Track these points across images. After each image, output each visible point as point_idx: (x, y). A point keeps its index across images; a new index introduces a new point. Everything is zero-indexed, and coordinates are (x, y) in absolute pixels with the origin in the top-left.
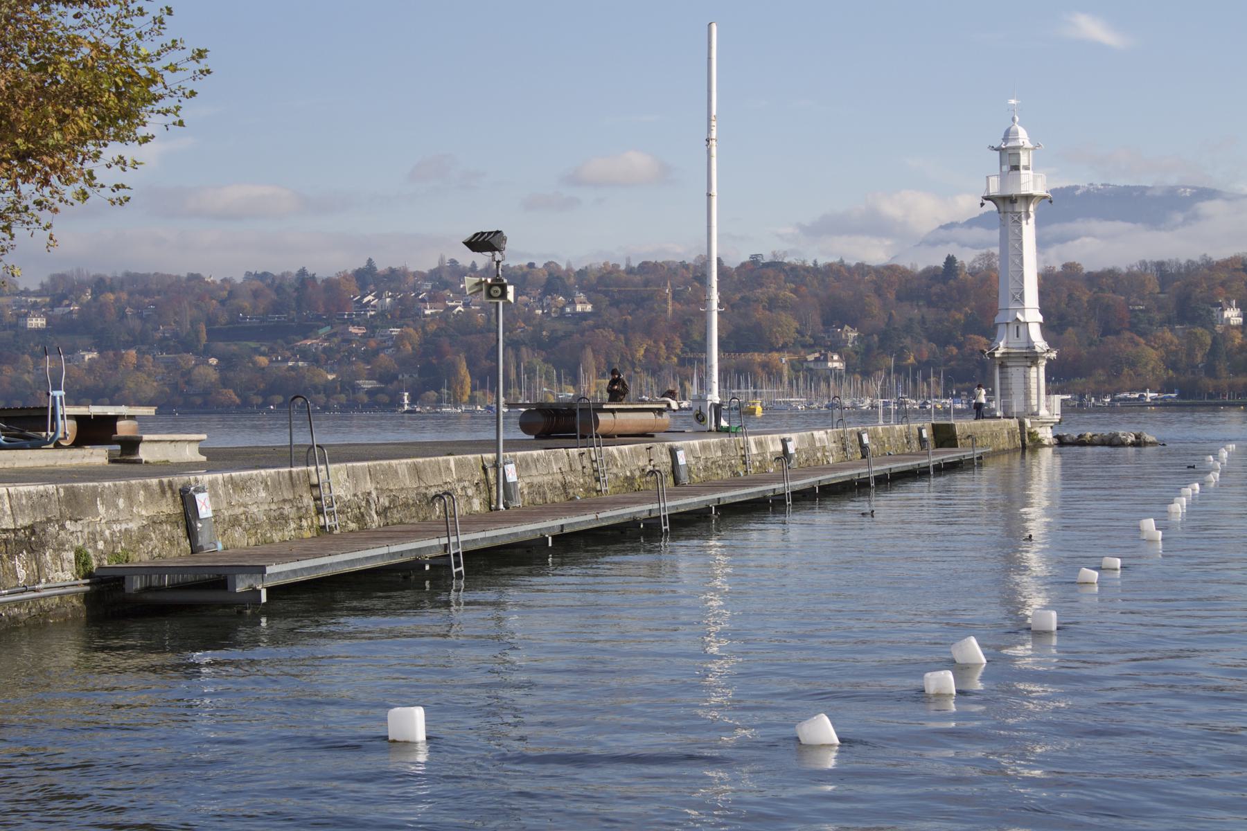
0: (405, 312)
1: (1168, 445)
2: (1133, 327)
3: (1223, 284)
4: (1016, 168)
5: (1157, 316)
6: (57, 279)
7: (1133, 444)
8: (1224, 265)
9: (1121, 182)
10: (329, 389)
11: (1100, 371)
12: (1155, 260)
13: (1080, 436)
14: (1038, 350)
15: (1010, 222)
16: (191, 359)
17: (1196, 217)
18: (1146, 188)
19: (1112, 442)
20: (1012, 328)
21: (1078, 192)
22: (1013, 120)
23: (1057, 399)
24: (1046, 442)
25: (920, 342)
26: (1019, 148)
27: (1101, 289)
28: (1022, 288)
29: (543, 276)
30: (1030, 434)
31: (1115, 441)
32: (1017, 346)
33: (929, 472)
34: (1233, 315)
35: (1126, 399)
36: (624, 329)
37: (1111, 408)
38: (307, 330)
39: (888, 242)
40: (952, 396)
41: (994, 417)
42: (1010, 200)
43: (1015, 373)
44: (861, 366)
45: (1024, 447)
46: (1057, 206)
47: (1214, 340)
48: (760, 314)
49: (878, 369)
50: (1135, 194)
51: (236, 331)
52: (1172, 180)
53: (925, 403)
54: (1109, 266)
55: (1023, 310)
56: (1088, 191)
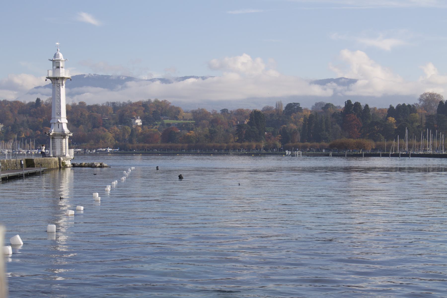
1: (112, 167)
2: (104, 125)
3: (135, 111)
4: (58, 67)
5: (112, 122)
7: (99, 167)
8: (136, 104)
9: (100, 74)
11: (92, 141)
12: (112, 101)
13: (81, 164)
14: (66, 133)
15: (56, 86)
17: (126, 87)
18: (109, 76)
19: (92, 166)
20: (57, 125)
21: (85, 77)
22: (58, 50)
23: (72, 151)
24: (68, 166)
25: (27, 129)
26: (60, 60)
27: (92, 111)
28: (60, 111)
30: (62, 163)
31: (93, 166)
32: (58, 131)
33: (23, 176)
34: (139, 122)
35: (101, 151)
37: (96, 154)
39: (15, 93)
40: (38, 149)
41: (50, 157)
43: (57, 141)
45: (60, 167)
46: (73, 82)
47: (132, 130)
49: (11, 139)
50: (105, 78)
52: (119, 74)
53: (28, 151)
54: (96, 103)
55: (60, 119)
56: (89, 76)
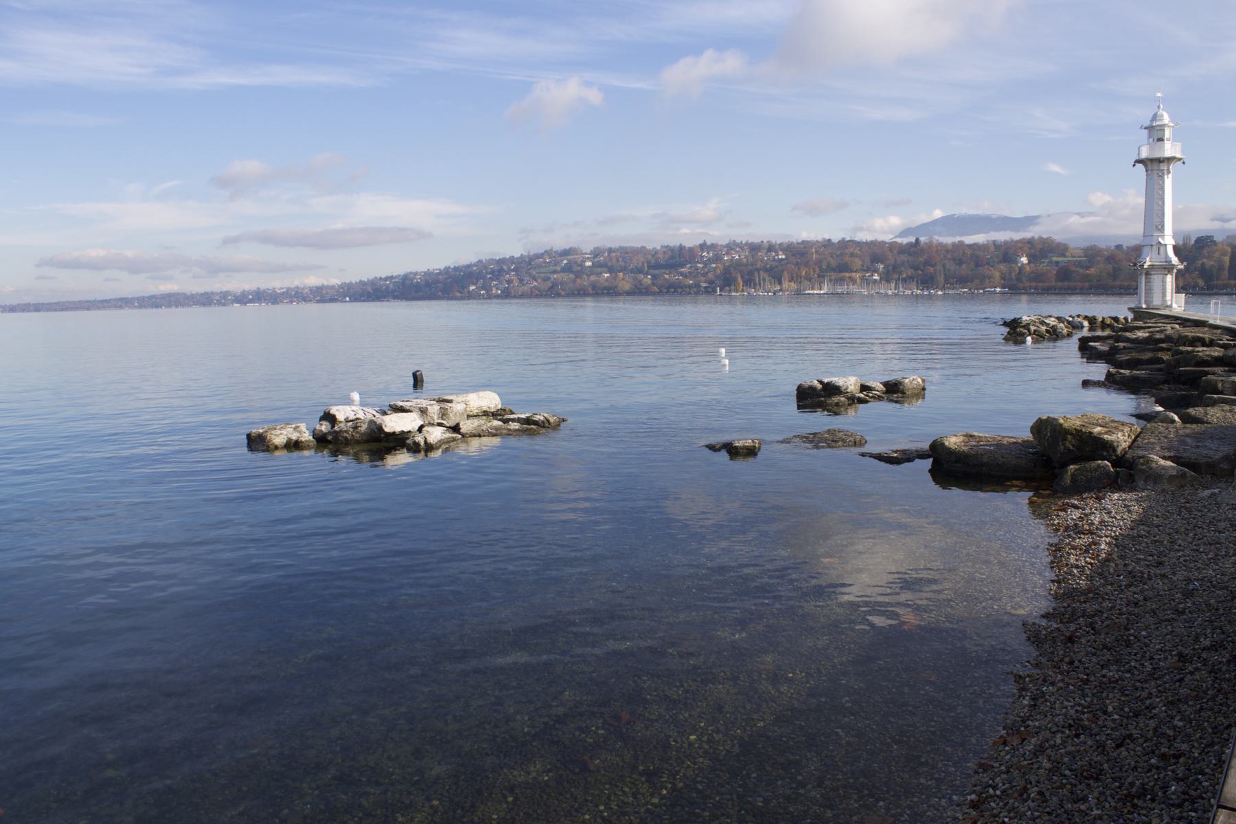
0: (717, 259)
4: (1161, 140)
6: (596, 249)
10: (690, 286)
16: (642, 276)
29: (767, 246)
34: (1024, 260)
36: (797, 264)
38: (682, 266)
42: (1160, 161)
43: (1156, 279)
44: (886, 278)
48: (847, 259)
51: (657, 266)
